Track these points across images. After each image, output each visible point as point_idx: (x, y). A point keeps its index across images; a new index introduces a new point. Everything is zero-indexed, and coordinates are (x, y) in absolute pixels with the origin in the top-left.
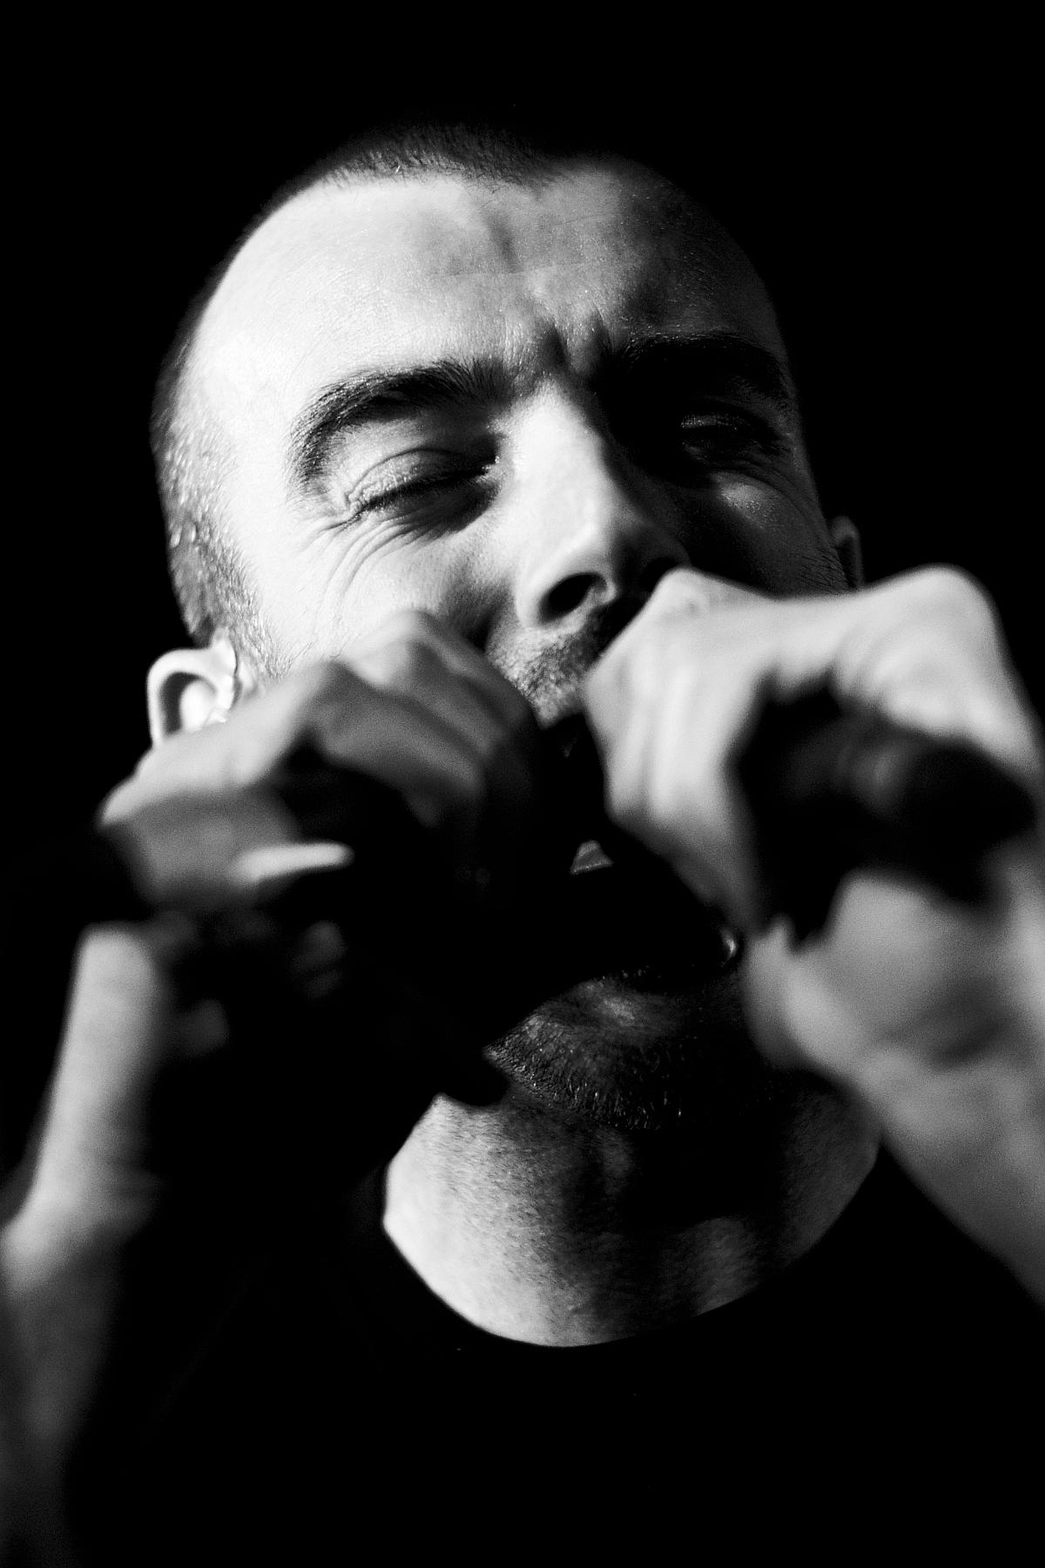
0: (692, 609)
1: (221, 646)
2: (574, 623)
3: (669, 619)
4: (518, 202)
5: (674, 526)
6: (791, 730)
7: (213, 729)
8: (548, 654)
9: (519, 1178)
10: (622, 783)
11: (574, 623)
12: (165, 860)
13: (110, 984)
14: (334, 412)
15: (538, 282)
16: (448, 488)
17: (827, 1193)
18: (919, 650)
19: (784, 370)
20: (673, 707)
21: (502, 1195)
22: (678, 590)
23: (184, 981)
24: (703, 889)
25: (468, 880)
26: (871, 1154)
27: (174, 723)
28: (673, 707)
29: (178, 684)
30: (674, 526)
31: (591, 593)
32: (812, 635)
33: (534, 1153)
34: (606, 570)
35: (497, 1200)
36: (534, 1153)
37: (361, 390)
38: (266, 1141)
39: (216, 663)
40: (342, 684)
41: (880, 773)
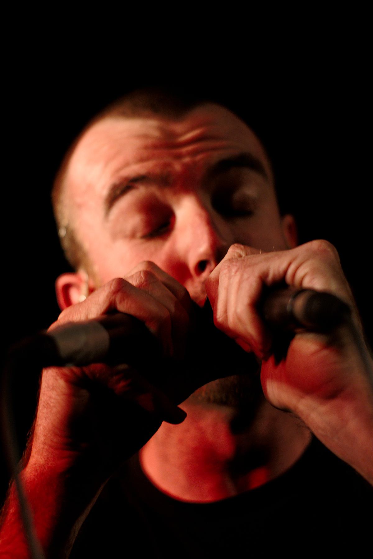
1: (82, 274)
3: (230, 260)
6: (269, 293)
7: (83, 304)
10: (219, 315)
12: (66, 346)
13: (52, 386)
16: (159, 223)
17: (294, 450)
18: (309, 267)
20: (233, 296)
23: (75, 384)
24: (247, 349)
25: (165, 348)
26: (307, 435)
27: (69, 303)
28: (233, 296)
29: (67, 287)
32: (276, 264)
37: (121, 183)
38: (106, 433)
39: (80, 280)
40: (122, 285)
41: (299, 305)
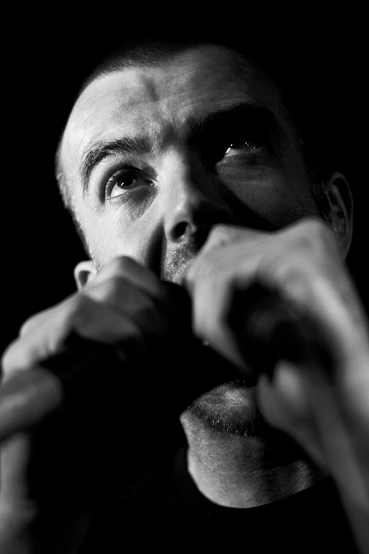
0: (223, 243)
2: (185, 239)
4: (156, 74)
5: (214, 208)
6: (250, 298)
8: (178, 251)
9: (218, 454)
11: (185, 239)
14: (119, 142)
15: (163, 106)
19: (349, 188)
20: (208, 280)
21: (214, 461)
22: (218, 235)
28: (208, 280)
30: (214, 208)
31: (187, 228)
33: (222, 444)
34: (188, 220)
35: (213, 463)
36: (222, 444)
